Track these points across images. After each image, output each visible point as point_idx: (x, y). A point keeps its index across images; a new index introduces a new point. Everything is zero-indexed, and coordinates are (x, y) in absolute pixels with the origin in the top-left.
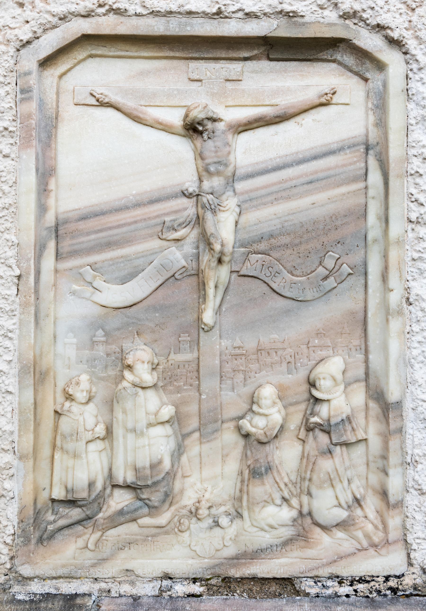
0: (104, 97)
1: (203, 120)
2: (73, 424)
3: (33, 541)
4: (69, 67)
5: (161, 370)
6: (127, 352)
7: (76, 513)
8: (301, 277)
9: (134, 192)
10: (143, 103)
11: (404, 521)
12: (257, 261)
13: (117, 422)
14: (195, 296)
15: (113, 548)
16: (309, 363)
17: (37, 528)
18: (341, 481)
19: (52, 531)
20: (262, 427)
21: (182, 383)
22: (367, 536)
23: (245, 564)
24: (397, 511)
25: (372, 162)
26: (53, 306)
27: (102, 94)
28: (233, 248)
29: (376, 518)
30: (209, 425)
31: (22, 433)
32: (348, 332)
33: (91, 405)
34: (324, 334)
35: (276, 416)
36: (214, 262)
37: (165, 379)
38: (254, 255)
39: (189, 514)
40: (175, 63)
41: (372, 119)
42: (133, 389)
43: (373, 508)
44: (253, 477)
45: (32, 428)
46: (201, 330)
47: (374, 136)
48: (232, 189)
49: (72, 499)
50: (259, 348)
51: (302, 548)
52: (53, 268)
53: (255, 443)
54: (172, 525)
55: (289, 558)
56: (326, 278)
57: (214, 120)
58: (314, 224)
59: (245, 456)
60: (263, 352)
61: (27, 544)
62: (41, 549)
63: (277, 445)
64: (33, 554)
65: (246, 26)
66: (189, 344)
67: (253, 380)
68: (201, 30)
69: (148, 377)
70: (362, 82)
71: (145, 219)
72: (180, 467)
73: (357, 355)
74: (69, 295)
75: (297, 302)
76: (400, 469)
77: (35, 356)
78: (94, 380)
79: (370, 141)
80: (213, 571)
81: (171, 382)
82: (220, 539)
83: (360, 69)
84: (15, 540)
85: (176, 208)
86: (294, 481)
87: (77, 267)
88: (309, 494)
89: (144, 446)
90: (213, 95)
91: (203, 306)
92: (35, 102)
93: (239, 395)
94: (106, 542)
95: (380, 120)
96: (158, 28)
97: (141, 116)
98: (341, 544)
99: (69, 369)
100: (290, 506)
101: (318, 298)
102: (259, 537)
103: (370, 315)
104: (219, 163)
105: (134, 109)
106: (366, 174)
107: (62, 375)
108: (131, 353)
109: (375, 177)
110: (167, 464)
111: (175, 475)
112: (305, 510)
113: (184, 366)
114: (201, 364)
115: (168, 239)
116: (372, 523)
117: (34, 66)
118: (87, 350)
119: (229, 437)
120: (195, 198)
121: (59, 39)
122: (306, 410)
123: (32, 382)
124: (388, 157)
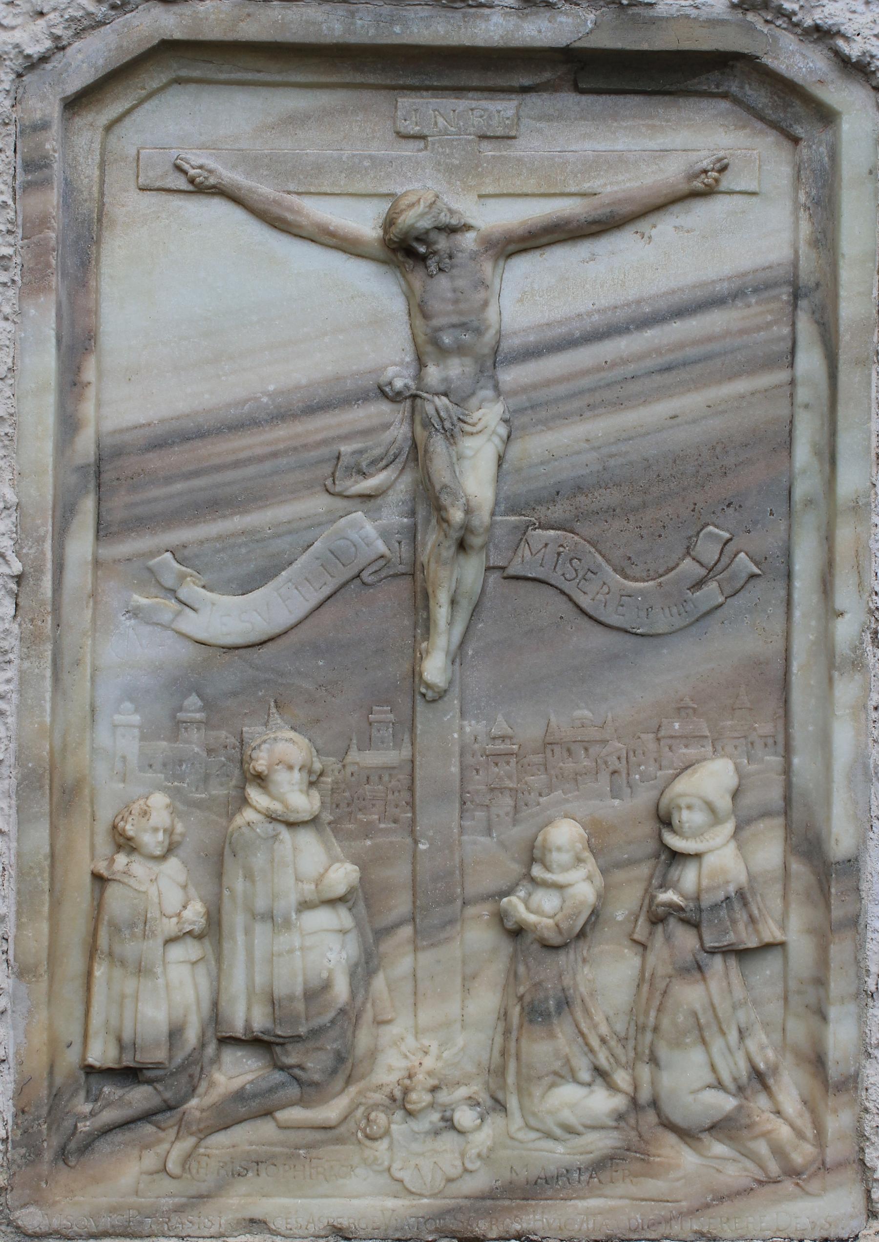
0: (206, 174)
1: (427, 232)
2: (135, 901)
3: (47, 1156)
4: (127, 106)
5: (330, 786)
6: (253, 745)
7: (140, 1097)
8: (644, 581)
9: (271, 388)
10: (292, 187)
11: (860, 1120)
12: (546, 545)
13: (233, 897)
14: (406, 622)
15: (223, 1172)
16: (659, 773)
17: (54, 1127)
18: (723, 1033)
19: (88, 1134)
20: (552, 913)
21: (377, 817)
22: (778, 1151)
23: (509, 1209)
24: (844, 1098)
25: (805, 327)
26: (89, 642)
27: (201, 167)
28: (493, 514)
29: (801, 1116)
30: (433, 912)
31: (24, 920)
32: (749, 705)
33: (173, 864)
34: (694, 710)
35: (583, 887)
36: (449, 547)
37: (337, 806)
38: (539, 531)
39: (387, 1102)
40: (367, 96)
41: (805, 228)
42: (267, 825)
43: (794, 1093)
44: (531, 1021)
45: (46, 909)
46: (418, 697)
47: (809, 266)
48: (490, 384)
49: (132, 1064)
50: (549, 739)
51: (636, 1176)
52: (90, 558)
53: (536, 946)
54: (351, 1124)
55: (606, 1197)
56: (699, 584)
57: (452, 230)
58: (675, 462)
59: (513, 976)
60: (557, 749)
61: (33, 1162)
62: (64, 1175)
63: (585, 952)
64: (47, 1183)
65: (525, 25)
66: (391, 730)
67: (534, 809)
68: (426, 32)
69: (302, 801)
70: (786, 144)
71: (295, 449)
72: (370, 1001)
73: (767, 758)
74: (124, 618)
75: (633, 638)
76: (852, 1008)
77: (52, 752)
78: (180, 806)
79: (801, 280)
80: (439, 1223)
81: (351, 813)
82: (457, 1155)
83: (782, 115)
84: (7, 1151)
85: (366, 424)
86: (623, 1035)
87: (143, 555)
88: (654, 1060)
89: (291, 951)
90: (451, 171)
91: (424, 645)
92: (55, 190)
93: (502, 844)
94: (206, 1158)
95: (824, 232)
96: (329, 28)
97: (289, 216)
98: (720, 1168)
99: (124, 781)
100: (611, 1086)
101: (681, 629)
102: (541, 1150)
103: (795, 667)
104: (463, 326)
105: (274, 201)
106: (793, 352)
107: (108, 795)
108: (264, 747)
109: (810, 361)
110: (341, 989)
111: (358, 1017)
112: (644, 1096)
113: (380, 778)
114: (419, 774)
115: (347, 493)
116: (792, 1126)
117: (55, 111)
118: (164, 739)
119: (478, 935)
120: (408, 403)
121: (110, 50)
122: (651, 877)
123: (47, 808)
124: (837, 320)
